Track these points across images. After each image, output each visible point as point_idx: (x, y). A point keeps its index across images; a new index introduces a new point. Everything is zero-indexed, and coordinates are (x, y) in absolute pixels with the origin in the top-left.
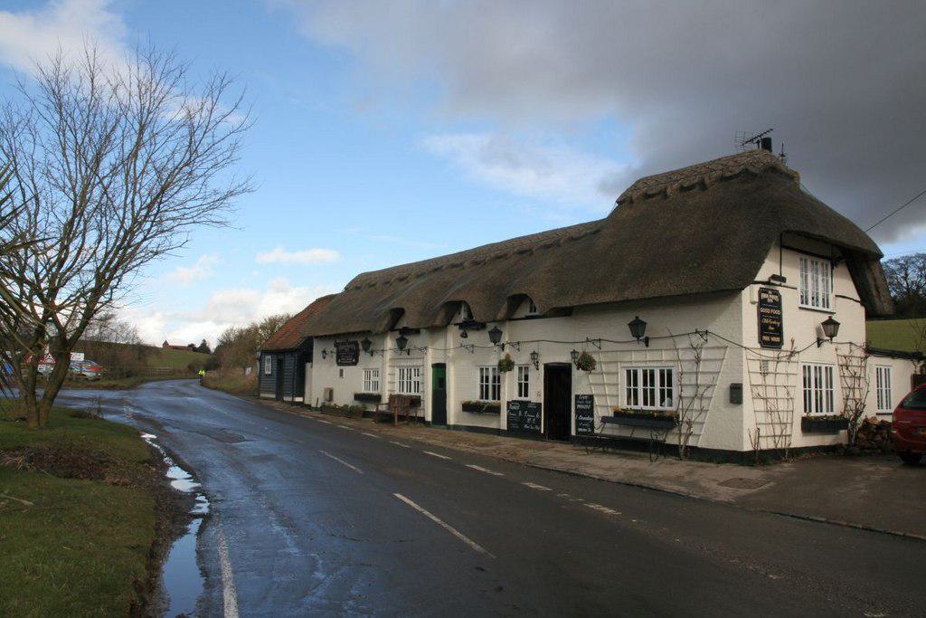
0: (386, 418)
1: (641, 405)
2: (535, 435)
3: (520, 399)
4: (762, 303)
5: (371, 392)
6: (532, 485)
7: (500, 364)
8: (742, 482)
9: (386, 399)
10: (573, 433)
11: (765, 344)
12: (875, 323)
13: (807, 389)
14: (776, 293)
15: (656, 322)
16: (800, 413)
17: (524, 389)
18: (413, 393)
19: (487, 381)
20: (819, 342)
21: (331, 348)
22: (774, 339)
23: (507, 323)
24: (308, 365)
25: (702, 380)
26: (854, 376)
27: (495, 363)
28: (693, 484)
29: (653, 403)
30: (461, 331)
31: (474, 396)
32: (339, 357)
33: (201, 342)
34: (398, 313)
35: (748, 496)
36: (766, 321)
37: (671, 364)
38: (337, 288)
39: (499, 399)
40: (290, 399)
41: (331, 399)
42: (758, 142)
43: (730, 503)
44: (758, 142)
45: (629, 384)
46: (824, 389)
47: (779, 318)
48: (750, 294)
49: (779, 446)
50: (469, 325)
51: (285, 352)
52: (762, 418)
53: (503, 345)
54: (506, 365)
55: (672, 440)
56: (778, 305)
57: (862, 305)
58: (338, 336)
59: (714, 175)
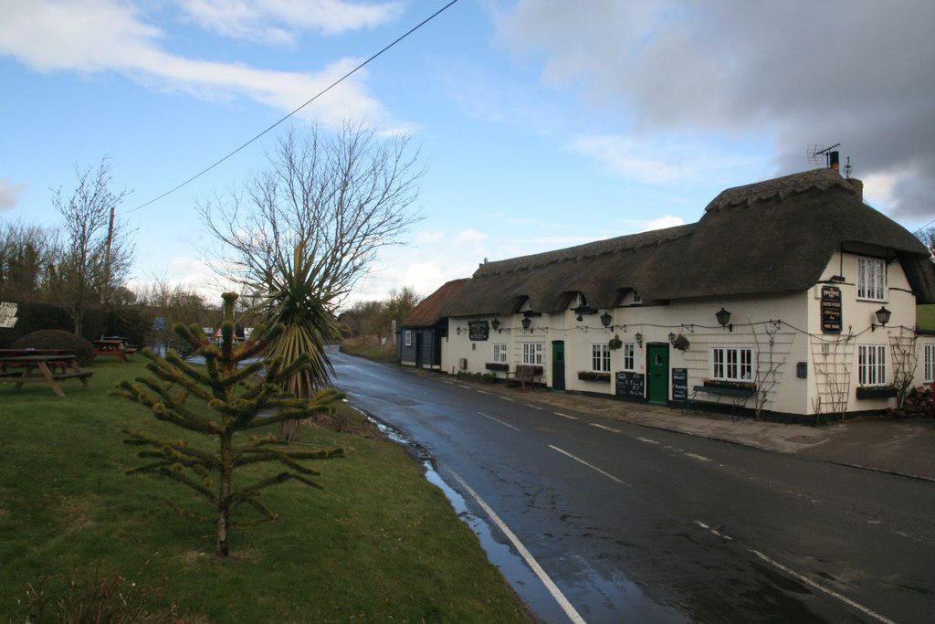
0: (514, 385)
1: (725, 378)
2: (639, 399)
3: (626, 370)
4: (825, 298)
5: (500, 362)
6: (644, 440)
7: (611, 342)
8: (805, 439)
9: (512, 369)
10: (671, 398)
11: (825, 331)
12: (922, 306)
13: (862, 365)
15: (738, 311)
16: (855, 384)
17: (629, 363)
18: (536, 364)
20: (873, 327)
21: (464, 325)
22: (834, 326)
23: (616, 310)
24: (444, 339)
25: (776, 359)
26: (904, 354)
27: (607, 342)
28: (765, 440)
29: (735, 376)
30: (577, 316)
31: (588, 368)
32: (471, 333)
34: (524, 299)
35: (807, 449)
36: (828, 312)
37: (751, 345)
38: (467, 271)
39: (609, 370)
40: (429, 367)
41: (465, 368)
42: (827, 155)
43: (793, 454)
44: (827, 155)
46: (877, 364)
47: (839, 310)
48: (814, 294)
49: (837, 411)
50: (581, 311)
51: (423, 328)
52: (822, 389)
53: (612, 327)
54: (616, 344)
55: (750, 404)
56: (838, 299)
57: (913, 294)
58: (471, 316)
59: (788, 190)
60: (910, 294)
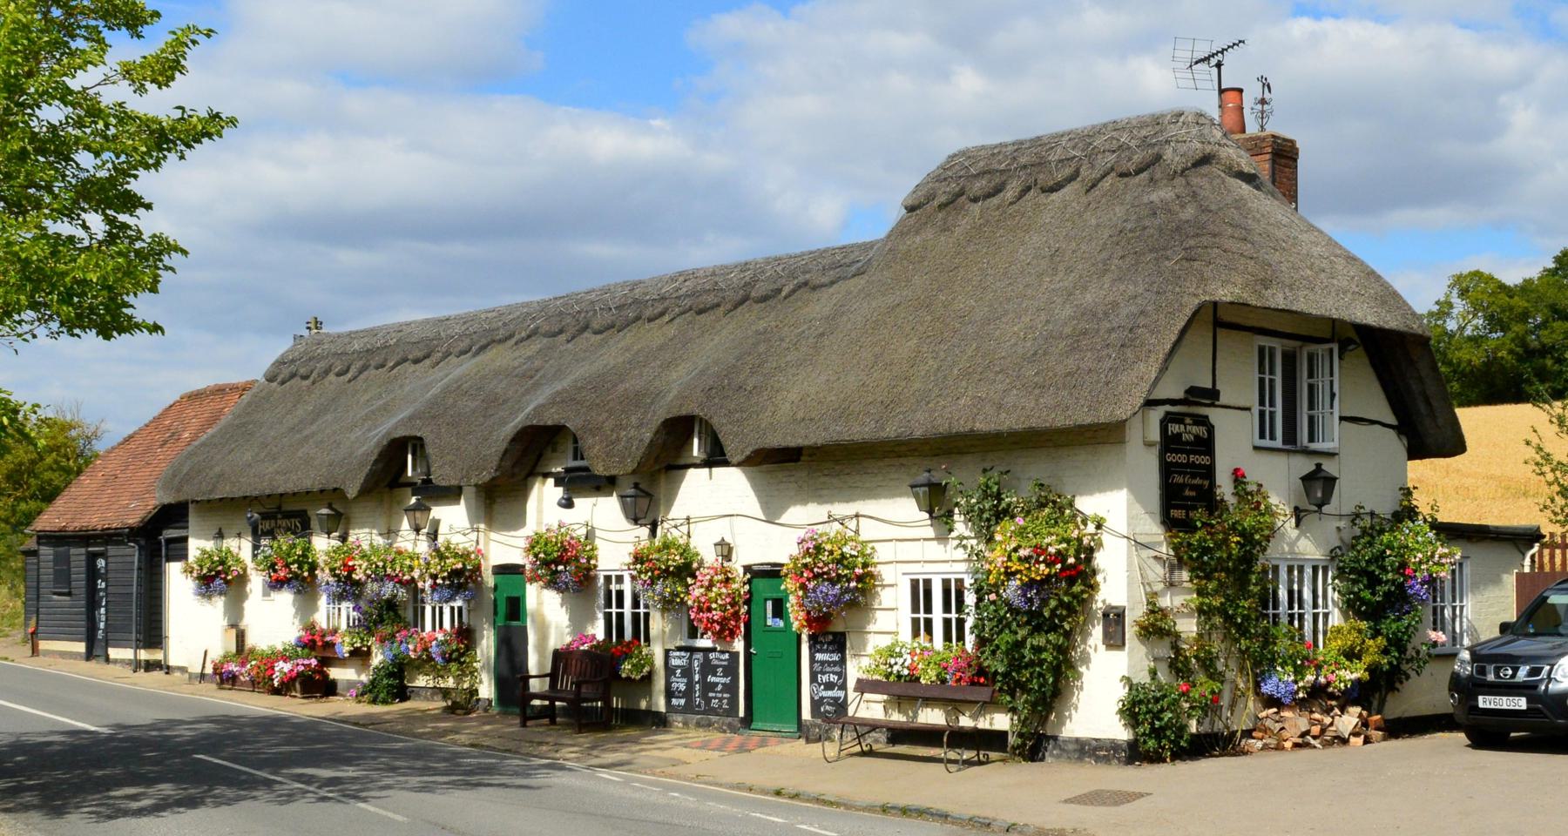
4: (1169, 443)
14: (1203, 421)
19: (620, 604)
30: (559, 492)
33: (275, 595)
36: (1179, 479)
45: (915, 609)
56: (1206, 445)
60: (1392, 433)
